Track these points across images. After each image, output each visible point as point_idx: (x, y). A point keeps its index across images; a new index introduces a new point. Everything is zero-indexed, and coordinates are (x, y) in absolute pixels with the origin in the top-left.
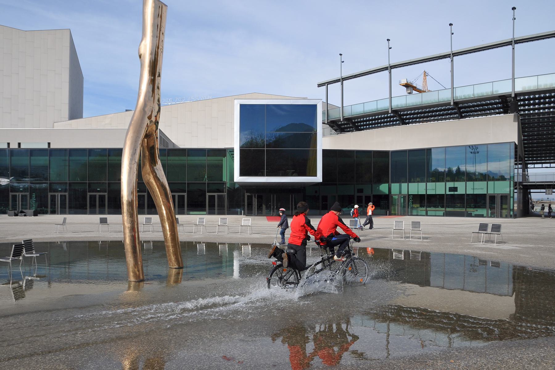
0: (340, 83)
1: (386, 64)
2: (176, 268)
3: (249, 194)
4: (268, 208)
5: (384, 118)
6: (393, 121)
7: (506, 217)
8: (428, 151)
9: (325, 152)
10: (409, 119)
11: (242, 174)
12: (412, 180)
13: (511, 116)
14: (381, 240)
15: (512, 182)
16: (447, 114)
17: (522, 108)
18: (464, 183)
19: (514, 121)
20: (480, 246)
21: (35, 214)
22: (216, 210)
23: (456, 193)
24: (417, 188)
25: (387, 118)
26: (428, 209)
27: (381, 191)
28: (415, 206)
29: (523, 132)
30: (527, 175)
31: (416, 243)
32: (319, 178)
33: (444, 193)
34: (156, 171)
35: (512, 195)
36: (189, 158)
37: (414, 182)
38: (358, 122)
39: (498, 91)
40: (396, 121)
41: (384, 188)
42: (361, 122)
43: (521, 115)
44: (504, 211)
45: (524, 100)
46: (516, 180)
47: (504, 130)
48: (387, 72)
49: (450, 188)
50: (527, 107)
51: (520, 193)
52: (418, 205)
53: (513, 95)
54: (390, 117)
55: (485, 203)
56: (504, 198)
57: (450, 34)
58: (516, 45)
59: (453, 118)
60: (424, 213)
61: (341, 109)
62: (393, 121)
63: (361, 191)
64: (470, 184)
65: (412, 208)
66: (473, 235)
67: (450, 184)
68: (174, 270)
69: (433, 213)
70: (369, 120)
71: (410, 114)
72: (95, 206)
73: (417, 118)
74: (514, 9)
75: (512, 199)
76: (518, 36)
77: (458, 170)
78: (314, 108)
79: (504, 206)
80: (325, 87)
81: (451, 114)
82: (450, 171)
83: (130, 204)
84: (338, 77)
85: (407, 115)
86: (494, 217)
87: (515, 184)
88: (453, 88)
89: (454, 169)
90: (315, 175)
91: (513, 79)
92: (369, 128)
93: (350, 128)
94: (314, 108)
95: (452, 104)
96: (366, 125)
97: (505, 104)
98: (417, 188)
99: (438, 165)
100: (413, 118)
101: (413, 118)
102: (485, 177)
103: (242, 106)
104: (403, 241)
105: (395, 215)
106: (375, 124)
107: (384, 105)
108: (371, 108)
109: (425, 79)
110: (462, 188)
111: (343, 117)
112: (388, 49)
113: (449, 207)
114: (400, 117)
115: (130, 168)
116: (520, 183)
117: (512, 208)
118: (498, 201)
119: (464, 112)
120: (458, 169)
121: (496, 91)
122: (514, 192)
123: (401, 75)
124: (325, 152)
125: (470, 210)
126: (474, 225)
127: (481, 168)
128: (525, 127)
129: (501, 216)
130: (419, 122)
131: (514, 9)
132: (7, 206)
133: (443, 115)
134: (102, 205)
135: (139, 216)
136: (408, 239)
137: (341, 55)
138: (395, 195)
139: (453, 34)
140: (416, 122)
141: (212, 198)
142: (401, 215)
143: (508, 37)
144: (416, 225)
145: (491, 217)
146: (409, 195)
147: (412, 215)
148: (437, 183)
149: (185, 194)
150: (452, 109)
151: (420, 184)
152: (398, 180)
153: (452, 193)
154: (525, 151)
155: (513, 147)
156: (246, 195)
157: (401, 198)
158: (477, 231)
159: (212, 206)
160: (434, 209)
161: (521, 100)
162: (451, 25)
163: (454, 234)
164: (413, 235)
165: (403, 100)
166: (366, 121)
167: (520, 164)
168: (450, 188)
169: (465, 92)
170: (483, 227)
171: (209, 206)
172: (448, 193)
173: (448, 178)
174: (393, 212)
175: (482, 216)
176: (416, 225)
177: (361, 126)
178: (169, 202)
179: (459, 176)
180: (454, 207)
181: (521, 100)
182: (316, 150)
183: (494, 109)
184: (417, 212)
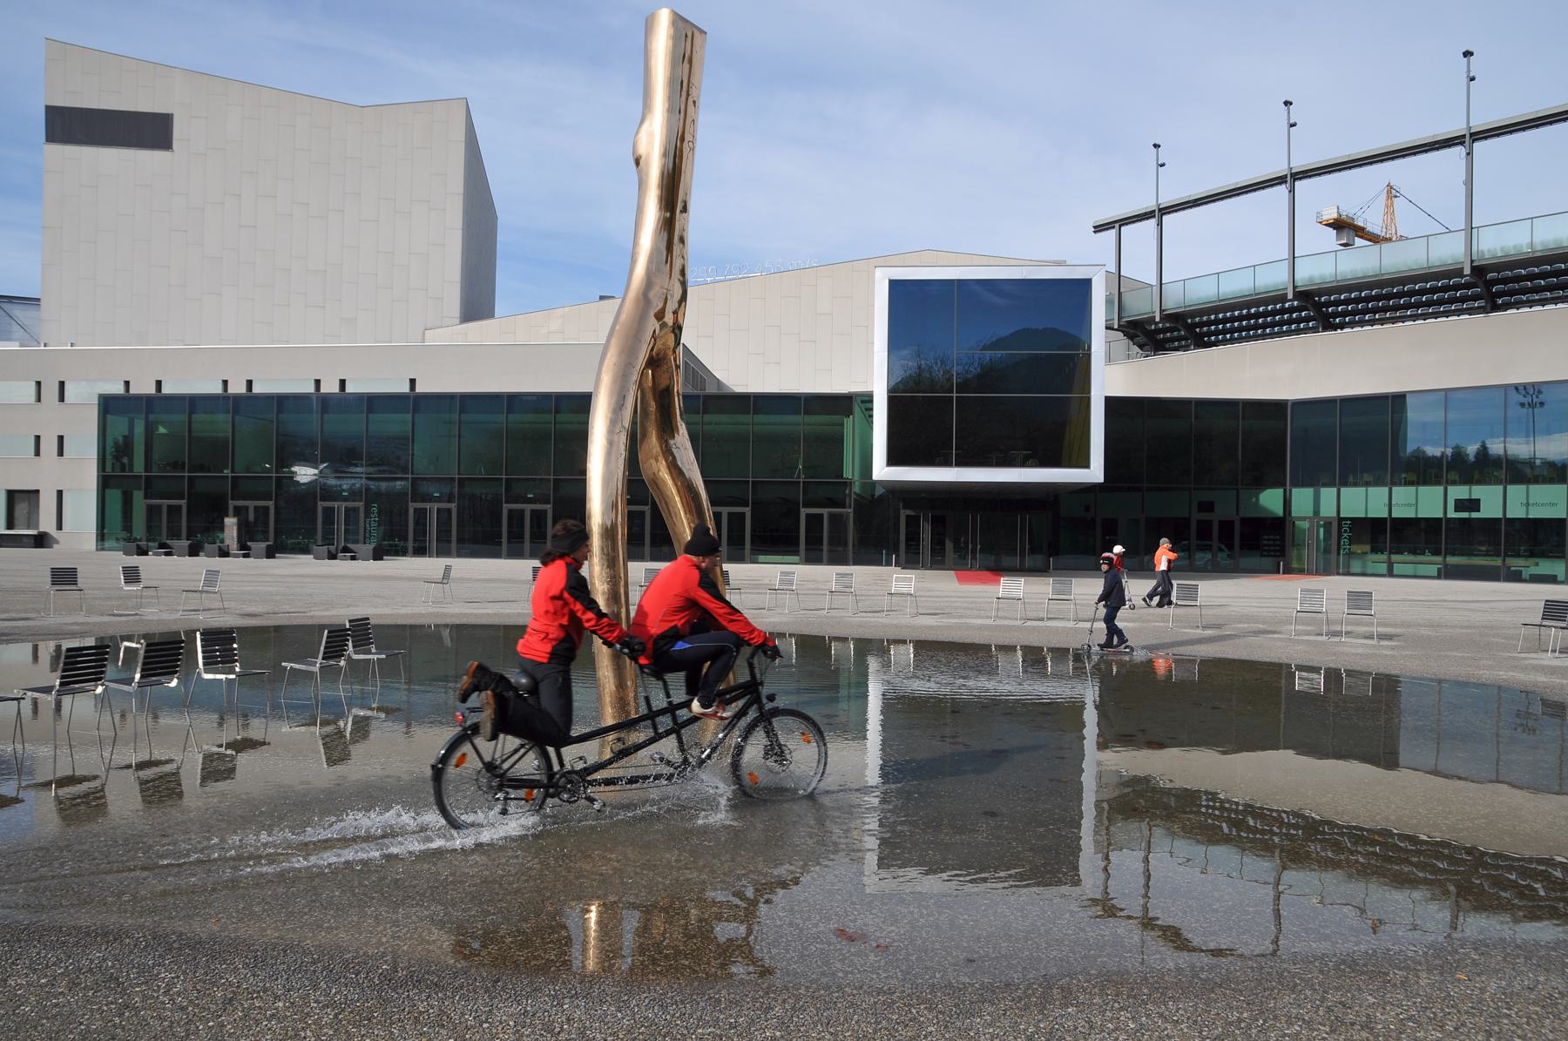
1: (1281, 169)
5: (1274, 313)
6: (1298, 321)
8: (1397, 401)
10: (1344, 314)
12: (1351, 479)
14: (1260, 639)
18: (1501, 488)
23: (1475, 515)
25: (1283, 311)
26: (1394, 557)
27: (1265, 510)
31: (1360, 650)
32: (1094, 473)
36: (760, 418)
37: (1355, 485)
40: (1307, 319)
41: (1271, 500)
48: (1282, 190)
52: (1367, 548)
54: (1292, 310)
57: (1465, 80)
59: (1470, 311)
60: (1383, 568)
61: (1156, 291)
63: (1207, 507)
64: (1516, 492)
65: (1350, 554)
67: (1459, 492)
69: (1409, 569)
70: (1233, 319)
71: (1347, 302)
77: (1483, 452)
80: (1112, 233)
81: (1463, 300)
83: (609, 533)
84: (1149, 204)
85: (1337, 303)
89: (1472, 449)
90: (1085, 464)
93: (1179, 339)
95: (1467, 271)
96: (1224, 332)
100: (1354, 313)
101: (1354, 313)
103: (895, 285)
104: (1323, 643)
105: (1301, 571)
106: (1248, 329)
107: (1274, 278)
108: (1237, 286)
109: (1390, 209)
110: (1492, 501)
111: (1162, 311)
113: (1453, 554)
114: (1317, 309)
119: (1501, 294)
120: (1483, 452)
124: (1112, 404)
125: (1516, 563)
126: (1527, 604)
130: (1372, 322)
132: (311, 533)
133: (1440, 302)
134: (838, 540)
137: (1156, 146)
138: (1304, 519)
139: (1473, 79)
140: (1362, 323)
142: (1318, 573)
144: (1359, 600)
146: (1341, 520)
147: (1348, 574)
148: (1421, 489)
149: (747, 511)
150: (1467, 286)
152: (1312, 478)
153: (1465, 515)
157: (1319, 526)
158: (1538, 620)
160: (1411, 558)
164: (1349, 628)
165: (1328, 261)
171: (807, 543)
172: (1452, 514)
173: (1453, 476)
174: (1295, 565)
176: (1359, 600)
177: (1210, 334)
179: (1485, 468)
180: (1470, 554)
182: (1089, 399)
184: (1364, 566)
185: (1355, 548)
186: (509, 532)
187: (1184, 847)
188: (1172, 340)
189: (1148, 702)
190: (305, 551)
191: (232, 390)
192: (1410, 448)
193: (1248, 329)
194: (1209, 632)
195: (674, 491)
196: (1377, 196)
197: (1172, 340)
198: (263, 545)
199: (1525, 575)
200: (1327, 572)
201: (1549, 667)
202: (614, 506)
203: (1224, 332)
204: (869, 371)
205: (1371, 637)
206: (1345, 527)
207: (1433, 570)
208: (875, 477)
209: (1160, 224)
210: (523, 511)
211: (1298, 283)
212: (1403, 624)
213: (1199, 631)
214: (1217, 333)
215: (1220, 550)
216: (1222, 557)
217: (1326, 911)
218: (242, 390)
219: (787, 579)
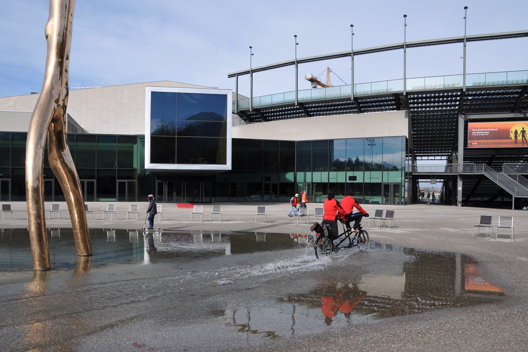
0: (249, 75)
2: (84, 256)
3: (159, 181)
4: (179, 194)
5: (291, 110)
6: (299, 113)
7: (398, 204)
8: (331, 142)
9: (234, 141)
10: (314, 111)
11: (153, 161)
12: (316, 169)
13: (402, 113)
14: (287, 226)
15: (403, 172)
16: (348, 109)
17: (412, 105)
22: (126, 197)
23: (355, 182)
24: (320, 177)
25: (294, 109)
28: (318, 193)
30: (416, 166)
32: (228, 166)
34: (64, 156)
35: (403, 184)
37: (318, 171)
38: (266, 113)
40: (302, 113)
41: (290, 176)
43: (411, 112)
45: (414, 99)
46: (407, 171)
52: (321, 193)
53: (405, 94)
54: (297, 109)
55: (380, 191)
56: (397, 187)
58: (407, 49)
59: (353, 112)
61: (250, 100)
63: (268, 179)
64: (367, 173)
65: (316, 195)
67: (350, 174)
68: (83, 257)
70: (277, 112)
71: (315, 107)
74: (405, 16)
75: (403, 188)
76: (409, 41)
78: (224, 97)
79: (397, 194)
80: (235, 78)
81: (351, 108)
82: (350, 161)
83: (36, 190)
85: (312, 107)
86: (388, 204)
87: (406, 174)
89: (354, 159)
90: (225, 163)
91: (405, 79)
92: (277, 119)
93: (258, 118)
94: (224, 97)
95: (352, 99)
96: (274, 116)
97: (398, 101)
98: (320, 177)
100: (317, 111)
101: (317, 111)
102: (380, 168)
103: (153, 94)
106: (282, 115)
107: (291, 98)
108: (278, 100)
109: (328, 75)
110: (361, 177)
111: (252, 107)
114: (305, 109)
116: (410, 173)
117: (403, 196)
118: (392, 189)
119: (362, 107)
121: (390, 89)
122: (405, 182)
123: (308, 70)
125: (367, 198)
127: (377, 159)
133: (344, 109)
138: (301, 183)
140: (319, 115)
143: (400, 42)
145: (385, 204)
146: (313, 183)
149: (95, 181)
150: (352, 104)
152: (303, 169)
153: (352, 182)
154: (414, 145)
155: (404, 141)
156: (157, 182)
157: (306, 186)
161: (411, 99)
165: (309, 93)
166: (274, 112)
167: (410, 156)
169: (364, 89)
172: (348, 181)
173: (348, 168)
175: (377, 203)
177: (269, 116)
178: (77, 188)
179: (358, 166)
181: (411, 99)
182: (226, 139)
184: (321, 199)
193: (282, 115)
194: (269, 224)
196: (324, 71)
203: (274, 116)
204: (143, 126)
206: (314, 186)
208: (146, 167)
209: (252, 76)
211: (299, 100)
214: (271, 116)
215: (273, 194)
216: (208, 199)
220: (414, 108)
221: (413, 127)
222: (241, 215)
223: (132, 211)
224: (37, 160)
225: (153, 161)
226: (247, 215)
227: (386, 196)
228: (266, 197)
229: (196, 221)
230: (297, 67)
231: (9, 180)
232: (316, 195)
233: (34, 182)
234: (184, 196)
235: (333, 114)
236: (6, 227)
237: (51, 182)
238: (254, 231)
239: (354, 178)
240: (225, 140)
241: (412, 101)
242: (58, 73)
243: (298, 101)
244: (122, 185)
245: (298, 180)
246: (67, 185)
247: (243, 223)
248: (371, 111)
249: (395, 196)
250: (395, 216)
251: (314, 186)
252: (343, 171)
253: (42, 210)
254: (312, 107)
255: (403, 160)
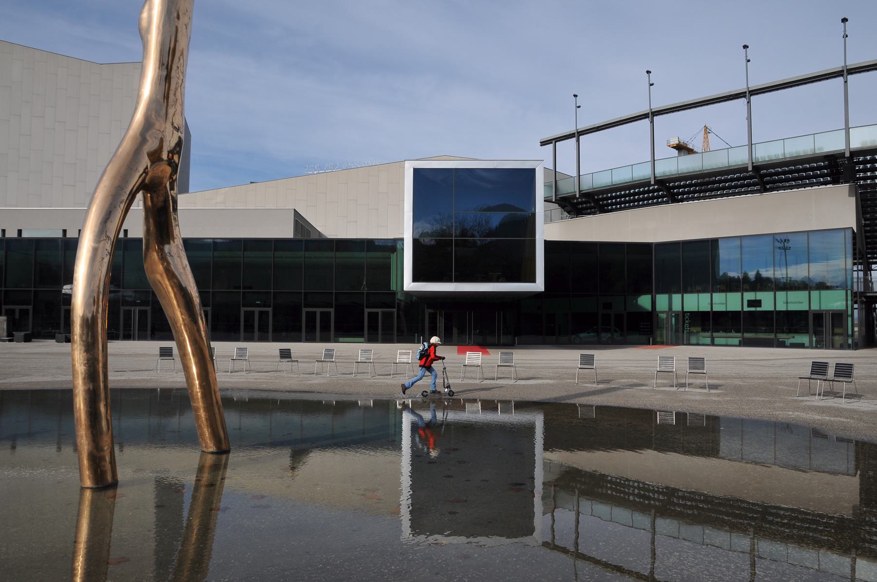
0: (574, 140)
1: (645, 109)
2: (212, 453)
3: (431, 311)
4: (462, 331)
5: (644, 193)
6: (658, 197)
7: (842, 347)
8: (712, 244)
9: (548, 244)
10: (683, 193)
11: (416, 279)
12: (689, 289)
13: (844, 188)
14: (634, 390)
15: (849, 292)
16: (742, 186)
17: (862, 175)
18: (772, 293)
19: (850, 195)
20: (816, 404)
21: (27, 339)
22: (380, 336)
23: (758, 309)
24: (697, 302)
25: (649, 192)
26: (715, 334)
27: (640, 307)
28: (694, 330)
29: (863, 214)
30: (871, 281)
31: (698, 398)
32: (539, 285)
33: (740, 309)
34: (169, 259)
35: (850, 313)
36: (339, 254)
37: (692, 292)
38: (603, 199)
39: (822, 149)
40: (663, 196)
41: (644, 301)
42: (607, 199)
43: (860, 186)
44: (836, 338)
45: (865, 162)
46: (855, 289)
47: (833, 209)
48: (647, 121)
49: (749, 301)
50: (869, 174)
51: (862, 309)
52: (699, 329)
53: (847, 155)
54: (654, 191)
55: (807, 325)
56: (838, 317)
57: (745, 61)
58: (849, 77)
59: (752, 192)
60: (708, 341)
61: (576, 180)
62: (658, 197)
63: (608, 306)
64: (781, 295)
65: (690, 333)
66: (800, 380)
67: (749, 296)
68: (210, 456)
69: (723, 341)
70: (621, 196)
71: (684, 186)
72: (314, 327)
73: (694, 192)
74: (844, 20)
75: (850, 319)
76: (852, 62)
77: (758, 275)
78: (530, 174)
79: (837, 330)
80: (551, 146)
81: (748, 185)
82: (746, 278)
83: (89, 324)
84: (572, 129)
85: (679, 187)
86: (821, 348)
87: (854, 295)
88: (751, 144)
89: (752, 275)
90: (533, 280)
91: (847, 129)
92: (621, 209)
93: (591, 208)
94: (530, 174)
95: (750, 169)
96: (616, 203)
97: (834, 168)
98: (697, 302)
99: (729, 265)
100: (689, 193)
101: (689, 193)
102: (803, 286)
103: (416, 171)
104: (674, 393)
105: (662, 343)
106: (629, 202)
107: (643, 172)
108: (622, 177)
109: (706, 138)
110: (768, 301)
111: (580, 191)
112: (648, 85)
113: (747, 332)
114: (667, 190)
115: (95, 251)
116: (861, 293)
117: (850, 332)
118: (828, 321)
119: (768, 183)
120: (758, 275)
121: (819, 149)
122: (853, 309)
123: (671, 129)
124: (548, 244)
125: (782, 337)
126: (791, 361)
127: (797, 272)
128: (866, 205)
129: (833, 347)
130: (699, 198)
131: (844, 20)
132: (58, 326)
133: (736, 187)
134: (325, 328)
135: (116, 347)
136: (682, 389)
137: (575, 96)
138: (663, 312)
139: (749, 61)
140: (693, 199)
141: (373, 317)
142: (672, 344)
143: (837, 65)
144: (697, 363)
145: (816, 347)
146: (684, 313)
147: (689, 344)
148: (728, 294)
149: (332, 310)
150: (750, 178)
151: (701, 295)
152: (669, 289)
153: (753, 309)
154: (867, 243)
155: (849, 235)
156: (427, 311)
157: (672, 317)
158: (808, 375)
159: (373, 328)
160: (724, 334)
161: (859, 163)
162: (745, 47)
163: (761, 378)
164: (691, 381)
165: (671, 165)
166: (616, 197)
167: (860, 264)
168: (749, 301)
169: (769, 151)
170: (819, 368)
171: (383, 330)
172: (746, 309)
173: (746, 286)
174: (659, 339)
175: (801, 346)
176: (697, 363)
177: (608, 205)
178: (196, 322)
179: (761, 284)
180: (756, 331)
181: (859, 163)
182: (535, 241)
183: (816, 176)
184: (698, 339)
185: (692, 329)
186: (245, 325)
187: (602, 509)
188: (587, 208)
189: (571, 423)
190: (51, 336)
191: (8, 235)
192: (721, 273)
193: (629, 202)
194: (601, 386)
195: (172, 295)
196: (698, 133)
197: (587, 208)
198: (23, 334)
199: (788, 342)
200: (677, 343)
201: (819, 407)
202: (95, 302)
203: (616, 203)
204: (401, 226)
205: (704, 387)
206: (687, 317)
207: (736, 341)
208: (405, 289)
209: (578, 141)
210: (253, 312)
211: (657, 174)
212: (724, 377)
213: (595, 385)
214: (612, 204)
215: (616, 331)
216: (616, 336)
217: (682, 546)
218: (15, 235)
219: (329, 354)
220: (865, 179)
221: (864, 213)
222: (557, 368)
223: (364, 360)
224: (97, 264)
225: (416, 279)
226: (567, 368)
227: (816, 333)
228: (605, 336)
229: (469, 378)
230: (652, 122)
231: (270, 310)
232: (690, 333)
233: (87, 305)
234: (470, 335)
235: (716, 196)
236: (163, 386)
237: (268, 312)
238: (572, 401)
239: (758, 303)
240: (534, 242)
241: (861, 166)
242: (160, 97)
243: (655, 177)
244: (373, 317)
245: (658, 308)
246: (177, 315)
247: (552, 385)
248: (785, 188)
249: (834, 334)
250: (856, 372)
251: (687, 317)
252: (737, 290)
253: (101, 365)
254: (679, 187)
255: (849, 272)
